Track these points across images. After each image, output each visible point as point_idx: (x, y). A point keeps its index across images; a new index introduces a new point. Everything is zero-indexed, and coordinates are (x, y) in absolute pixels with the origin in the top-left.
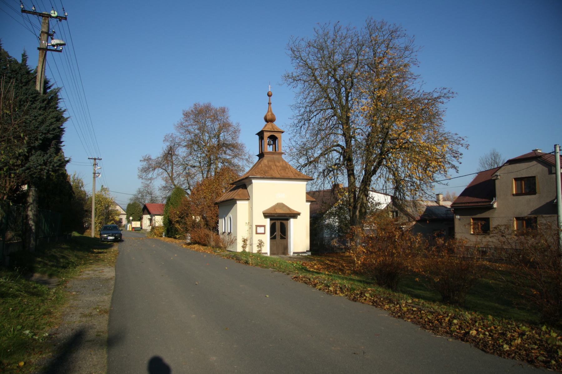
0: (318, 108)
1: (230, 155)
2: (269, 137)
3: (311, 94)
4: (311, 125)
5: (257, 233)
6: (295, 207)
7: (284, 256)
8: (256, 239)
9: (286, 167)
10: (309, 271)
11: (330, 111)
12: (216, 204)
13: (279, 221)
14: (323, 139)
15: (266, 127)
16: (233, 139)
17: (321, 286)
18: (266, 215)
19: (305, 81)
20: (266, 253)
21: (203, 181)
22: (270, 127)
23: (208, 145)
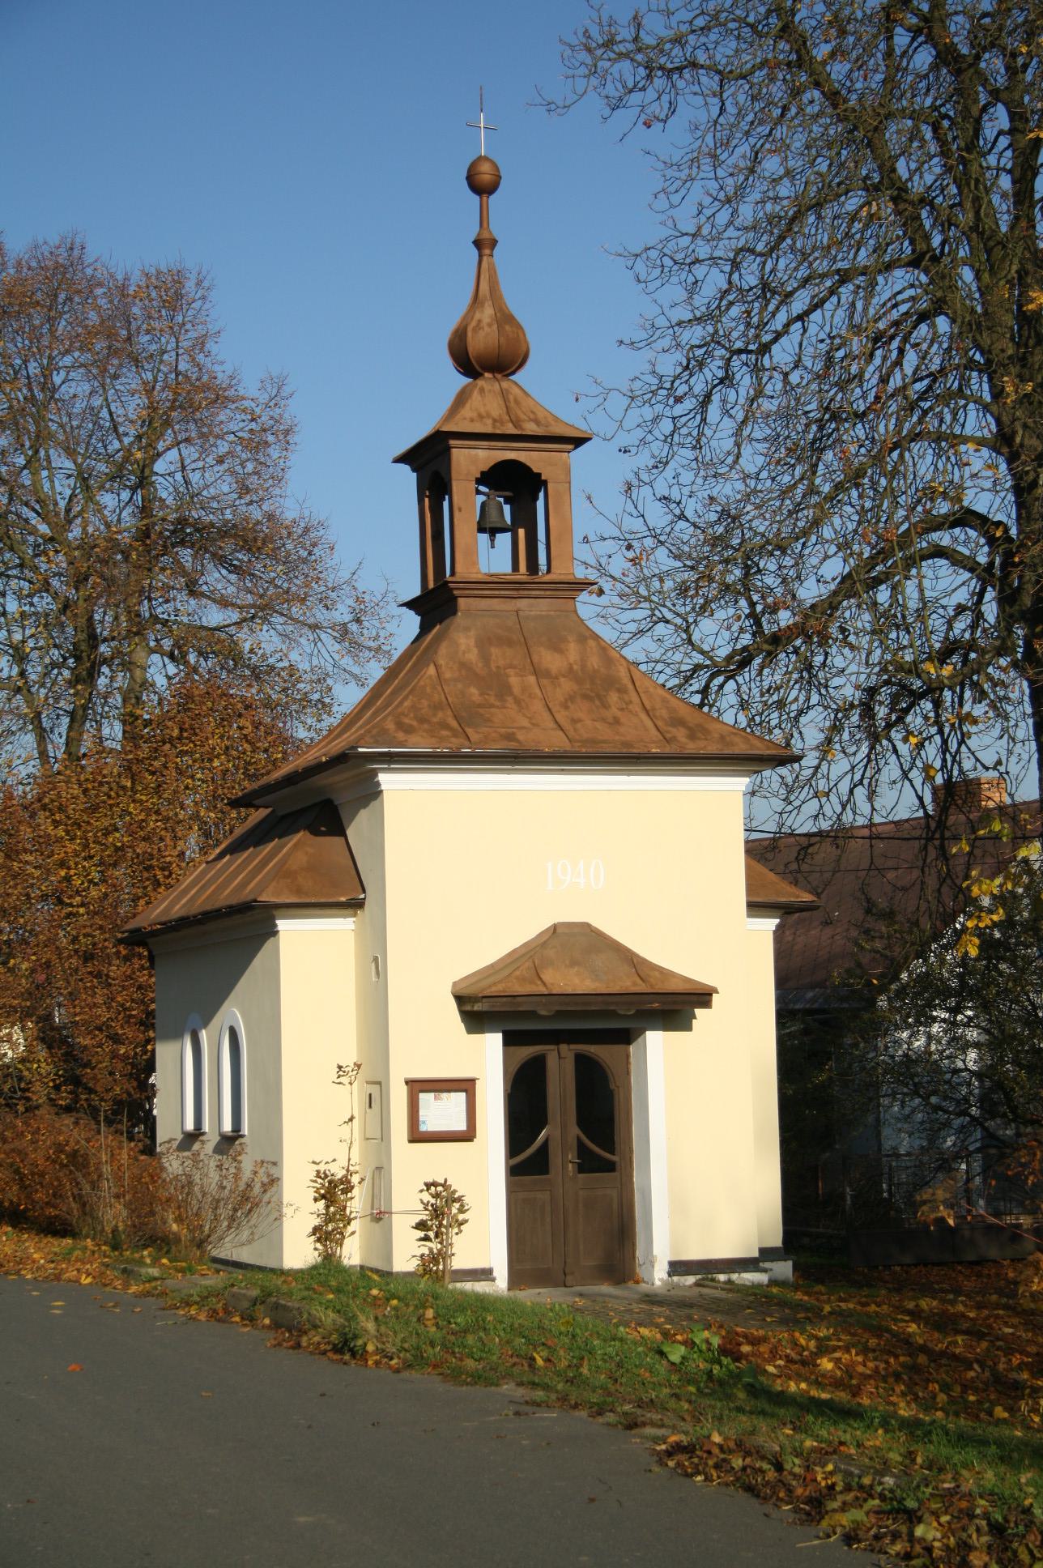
0: (822, 266)
1: (224, 603)
2: (487, 476)
3: (771, 165)
4: (774, 386)
5: (417, 1136)
6: (669, 948)
7: (606, 1289)
8: (413, 1169)
9: (603, 679)
10: (781, 1399)
11: (900, 285)
12: (137, 938)
13: (570, 1044)
14: (855, 477)
15: (466, 412)
16: (244, 490)
17: (858, 1515)
18: (477, 1009)
19: (724, 77)
20: (486, 1274)
21: (49, 781)
22: (495, 407)
23: (75, 533)
